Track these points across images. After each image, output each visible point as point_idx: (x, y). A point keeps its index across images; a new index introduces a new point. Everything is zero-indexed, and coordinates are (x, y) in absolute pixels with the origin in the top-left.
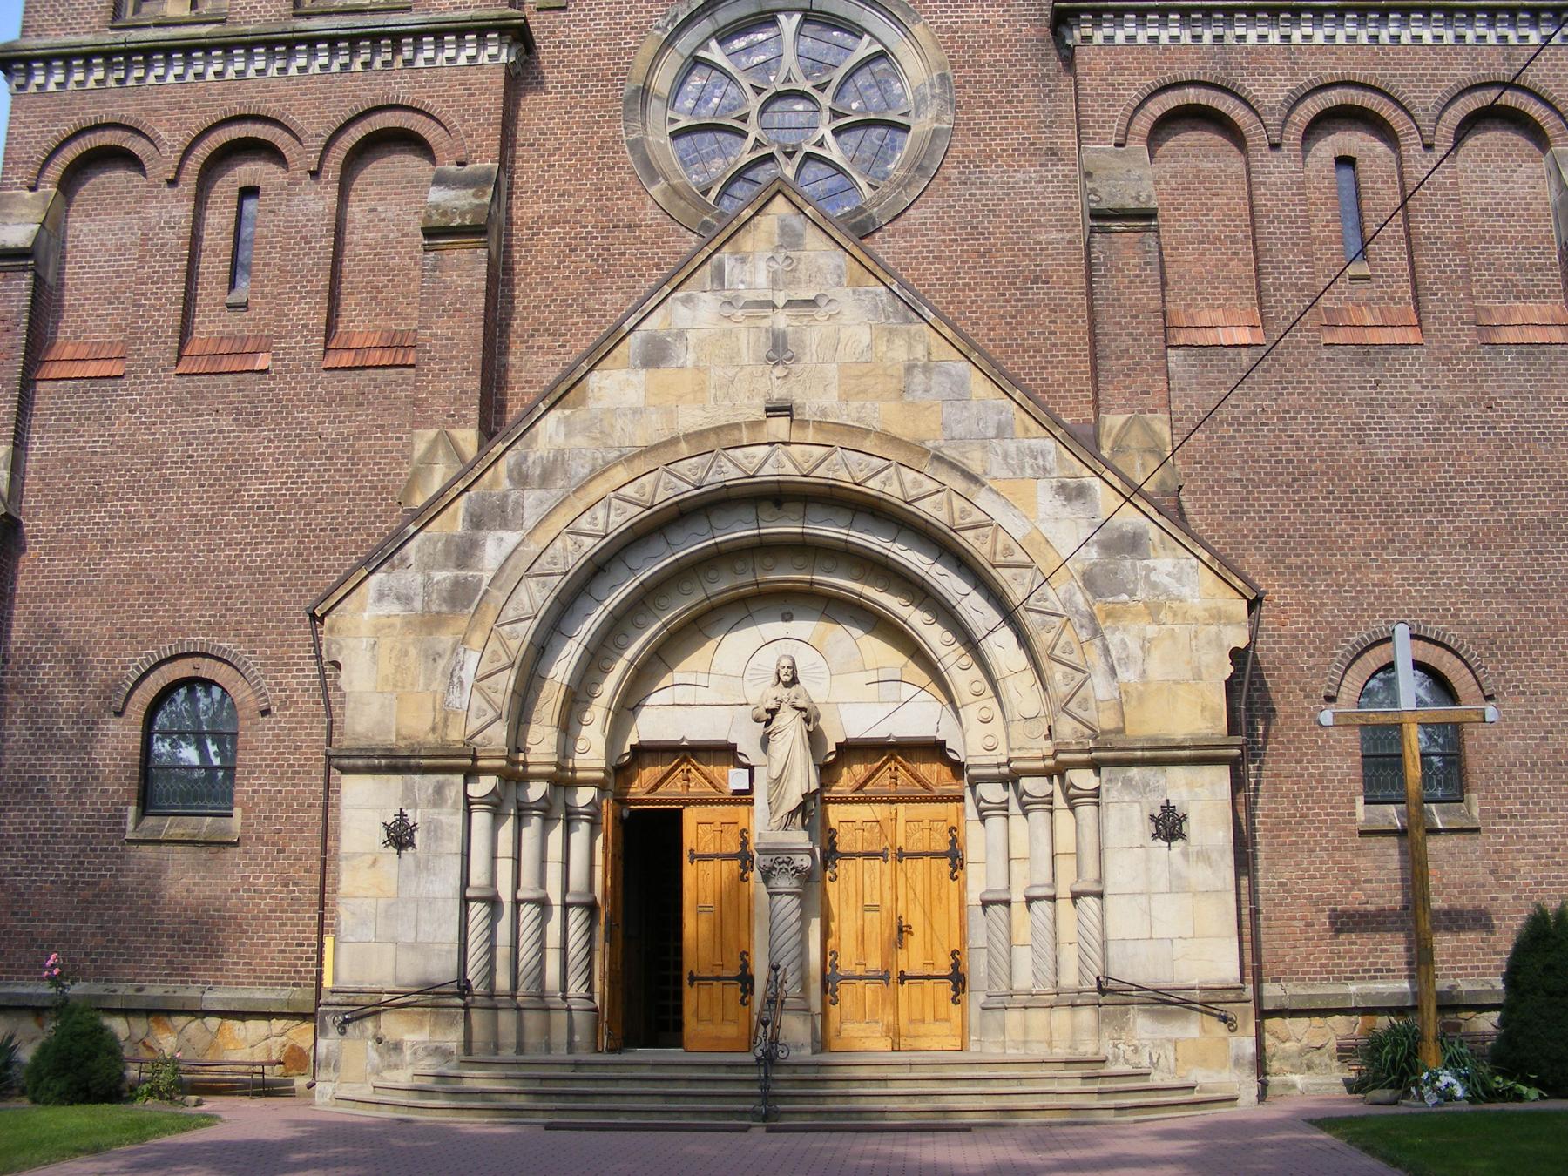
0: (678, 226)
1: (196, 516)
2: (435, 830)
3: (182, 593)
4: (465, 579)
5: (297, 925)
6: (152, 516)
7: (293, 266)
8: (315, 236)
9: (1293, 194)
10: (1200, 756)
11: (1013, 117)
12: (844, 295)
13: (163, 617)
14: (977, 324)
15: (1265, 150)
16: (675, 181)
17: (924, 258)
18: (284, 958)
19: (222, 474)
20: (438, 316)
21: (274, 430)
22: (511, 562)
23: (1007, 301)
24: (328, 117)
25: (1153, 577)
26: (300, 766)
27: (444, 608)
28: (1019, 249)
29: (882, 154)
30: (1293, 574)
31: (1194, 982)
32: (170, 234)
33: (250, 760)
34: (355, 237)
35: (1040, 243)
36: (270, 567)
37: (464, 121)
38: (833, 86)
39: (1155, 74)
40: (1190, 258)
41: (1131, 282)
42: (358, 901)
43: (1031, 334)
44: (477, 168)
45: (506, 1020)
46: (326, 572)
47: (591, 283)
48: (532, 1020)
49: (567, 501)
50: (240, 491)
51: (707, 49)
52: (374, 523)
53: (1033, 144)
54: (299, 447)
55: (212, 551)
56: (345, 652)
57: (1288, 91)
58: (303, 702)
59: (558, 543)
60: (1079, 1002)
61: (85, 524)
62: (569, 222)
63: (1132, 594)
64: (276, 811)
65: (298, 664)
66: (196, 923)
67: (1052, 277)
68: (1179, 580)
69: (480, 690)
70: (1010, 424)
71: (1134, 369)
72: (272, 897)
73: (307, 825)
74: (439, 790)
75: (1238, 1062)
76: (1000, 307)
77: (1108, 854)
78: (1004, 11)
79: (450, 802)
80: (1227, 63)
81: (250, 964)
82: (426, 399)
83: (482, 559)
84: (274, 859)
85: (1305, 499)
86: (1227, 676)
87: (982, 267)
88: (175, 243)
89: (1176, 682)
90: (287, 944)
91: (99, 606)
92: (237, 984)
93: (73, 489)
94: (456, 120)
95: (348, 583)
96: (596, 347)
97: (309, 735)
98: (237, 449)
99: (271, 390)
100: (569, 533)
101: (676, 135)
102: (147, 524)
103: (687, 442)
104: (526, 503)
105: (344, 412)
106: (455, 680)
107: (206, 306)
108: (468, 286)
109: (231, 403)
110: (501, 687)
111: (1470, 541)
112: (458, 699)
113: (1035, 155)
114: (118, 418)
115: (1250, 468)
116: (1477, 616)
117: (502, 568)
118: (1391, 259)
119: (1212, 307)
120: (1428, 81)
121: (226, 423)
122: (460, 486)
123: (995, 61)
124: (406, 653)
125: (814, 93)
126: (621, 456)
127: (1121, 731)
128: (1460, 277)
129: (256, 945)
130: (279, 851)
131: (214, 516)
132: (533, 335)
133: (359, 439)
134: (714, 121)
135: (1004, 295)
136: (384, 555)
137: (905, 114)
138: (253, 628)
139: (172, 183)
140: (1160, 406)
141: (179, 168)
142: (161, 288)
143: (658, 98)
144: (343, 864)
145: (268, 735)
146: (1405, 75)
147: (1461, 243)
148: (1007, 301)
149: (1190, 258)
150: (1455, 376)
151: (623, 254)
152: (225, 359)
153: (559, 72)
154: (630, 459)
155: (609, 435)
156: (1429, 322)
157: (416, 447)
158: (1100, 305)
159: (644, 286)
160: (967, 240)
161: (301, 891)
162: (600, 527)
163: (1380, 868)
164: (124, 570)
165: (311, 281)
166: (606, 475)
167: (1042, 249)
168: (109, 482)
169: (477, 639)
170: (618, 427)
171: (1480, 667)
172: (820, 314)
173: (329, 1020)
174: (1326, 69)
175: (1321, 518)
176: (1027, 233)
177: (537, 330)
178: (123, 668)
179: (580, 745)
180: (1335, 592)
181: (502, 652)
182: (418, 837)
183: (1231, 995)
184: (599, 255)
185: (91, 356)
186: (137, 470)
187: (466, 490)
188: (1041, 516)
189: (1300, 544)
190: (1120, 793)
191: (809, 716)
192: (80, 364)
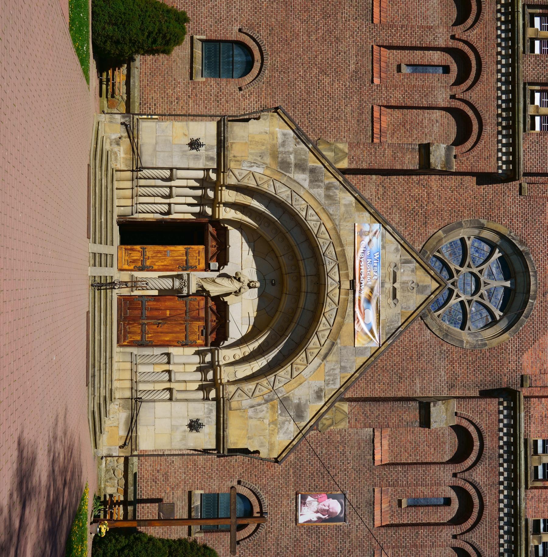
0: (425, 241)
1: (316, 57)
2: (197, 157)
3: (286, 54)
5: (162, 103)
6: (316, 39)
7: (416, 91)
8: (427, 99)
9: (435, 481)
10: (220, 437)
11: (468, 372)
12: (398, 310)
13: (277, 46)
15: (454, 471)
16: (444, 240)
17: (410, 336)
19: (333, 67)
20: (393, 151)
21: (349, 87)
22: (297, 185)
23: (392, 367)
24: (478, 100)
25: (287, 423)
26: (221, 103)
27: (280, 159)
28: (413, 372)
29: (453, 321)
30: (286, 471)
31: (139, 433)
32: (431, 38)
34: (426, 114)
35: (415, 380)
36: (296, 88)
37: (474, 157)
38: (482, 301)
39: (486, 429)
40: (409, 438)
41: (400, 416)
42: (171, 129)
43: (379, 375)
44: (453, 163)
45: (128, 184)
46: (293, 111)
47: (403, 209)
48: (128, 193)
49: (319, 205)
50: (326, 74)
51: (499, 252)
52: (312, 128)
53: (456, 379)
54: (342, 98)
55: (302, 65)
56: (264, 121)
57: (479, 483)
59: (304, 202)
60: (133, 391)
61: (314, 12)
62: (429, 199)
63: (281, 415)
64: (204, 94)
65: (259, 101)
66: (162, 64)
68: (285, 432)
69: (248, 174)
70: (346, 371)
71: (365, 415)
73: (199, 106)
74: (212, 159)
75: (110, 449)
76: (390, 364)
77: (186, 403)
78: (514, 370)
79: (208, 163)
80: (491, 458)
82: (360, 148)
83: (298, 173)
85: (314, 477)
86: (250, 449)
87: (406, 358)
88: (428, 41)
89: (247, 430)
90: (155, 100)
91: (282, 20)
92: (140, 81)
93: (328, 6)
94: (474, 154)
95: (290, 121)
96: (379, 215)
98: (342, 72)
99: (365, 85)
100: (307, 206)
101: (462, 240)
102: (313, 38)
103: (341, 250)
104: (319, 189)
105: (355, 115)
106: (253, 164)
107: (400, 55)
108: (405, 162)
109: (360, 69)
110: (250, 182)
111: (297, 540)
112: (245, 166)
113: (452, 379)
114: (356, 22)
115: (326, 457)
116: (269, 540)
117: (295, 181)
118: (408, 517)
119: (389, 445)
120: (484, 540)
121: (353, 67)
122: (326, 164)
123: (492, 366)
124: (263, 145)
125: (479, 294)
127: (230, 409)
128: (401, 544)
129: (155, 88)
131: (316, 64)
132: (383, 186)
133: (345, 121)
134: (468, 254)
135: (395, 365)
136: (300, 136)
137: (469, 329)
138: (273, 83)
139: (453, 37)
140: (351, 425)
141: (460, 40)
142: (409, 36)
143: (479, 233)
144: (185, 123)
146: (486, 530)
147: (415, 546)
148: (392, 367)
149: (409, 438)
150: (361, 539)
151: (415, 221)
152: (378, 65)
153: (492, 193)
154: (335, 229)
155: (345, 221)
156: (383, 530)
157: (341, 144)
159: (401, 229)
161: (175, 104)
162: (309, 218)
163: (177, 499)
164: (296, 29)
165: (409, 98)
168: (331, 20)
169: (268, 172)
170: (348, 224)
171: (250, 540)
172: (390, 300)
173: (127, 119)
174: (489, 498)
175: (307, 482)
176: (419, 375)
177: (385, 188)
179: (228, 209)
180: (279, 486)
181: (263, 181)
182: (194, 151)
183: (134, 447)
184: (415, 211)
185: (382, 9)
186: (335, 32)
187: (325, 167)
188: (310, 382)
189: (297, 474)
190: (207, 408)
191: (237, 293)
192: (378, 4)
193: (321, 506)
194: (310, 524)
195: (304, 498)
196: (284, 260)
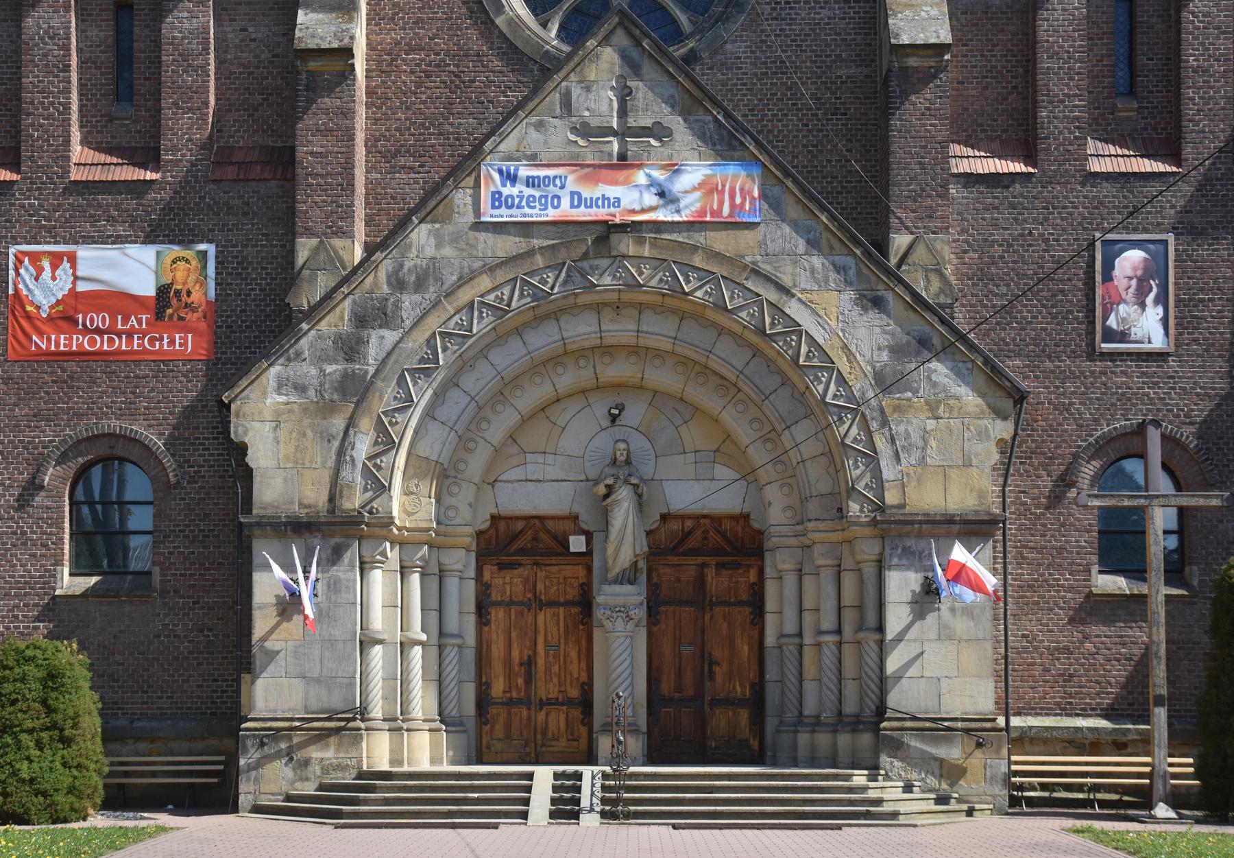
4: (353, 371)
14: (784, 152)
18: (202, 692)
23: (809, 131)
26: (209, 531)
27: (336, 397)
33: (165, 526)
35: (841, 77)
40: (974, 92)
56: (250, 434)
58: (209, 477)
63: (915, 392)
64: (190, 569)
66: (123, 664)
67: (850, 109)
72: (189, 642)
73: (218, 580)
81: (172, 697)
84: (190, 609)
87: (789, 99)
90: (204, 680)
97: (215, 504)
103: (542, 254)
118: (1157, 92)
124: (305, 435)
126: (484, 266)
127: (903, 506)
130: (194, 603)
133: (246, 246)
145: (180, 504)
150: (1208, 201)
158: (894, 136)
160: (776, 73)
166: (472, 282)
167: (842, 82)
176: (829, 68)
178: (44, 447)
193: (1130, 296)
194: (1172, 322)
195: (1109, 335)
196: (566, 379)
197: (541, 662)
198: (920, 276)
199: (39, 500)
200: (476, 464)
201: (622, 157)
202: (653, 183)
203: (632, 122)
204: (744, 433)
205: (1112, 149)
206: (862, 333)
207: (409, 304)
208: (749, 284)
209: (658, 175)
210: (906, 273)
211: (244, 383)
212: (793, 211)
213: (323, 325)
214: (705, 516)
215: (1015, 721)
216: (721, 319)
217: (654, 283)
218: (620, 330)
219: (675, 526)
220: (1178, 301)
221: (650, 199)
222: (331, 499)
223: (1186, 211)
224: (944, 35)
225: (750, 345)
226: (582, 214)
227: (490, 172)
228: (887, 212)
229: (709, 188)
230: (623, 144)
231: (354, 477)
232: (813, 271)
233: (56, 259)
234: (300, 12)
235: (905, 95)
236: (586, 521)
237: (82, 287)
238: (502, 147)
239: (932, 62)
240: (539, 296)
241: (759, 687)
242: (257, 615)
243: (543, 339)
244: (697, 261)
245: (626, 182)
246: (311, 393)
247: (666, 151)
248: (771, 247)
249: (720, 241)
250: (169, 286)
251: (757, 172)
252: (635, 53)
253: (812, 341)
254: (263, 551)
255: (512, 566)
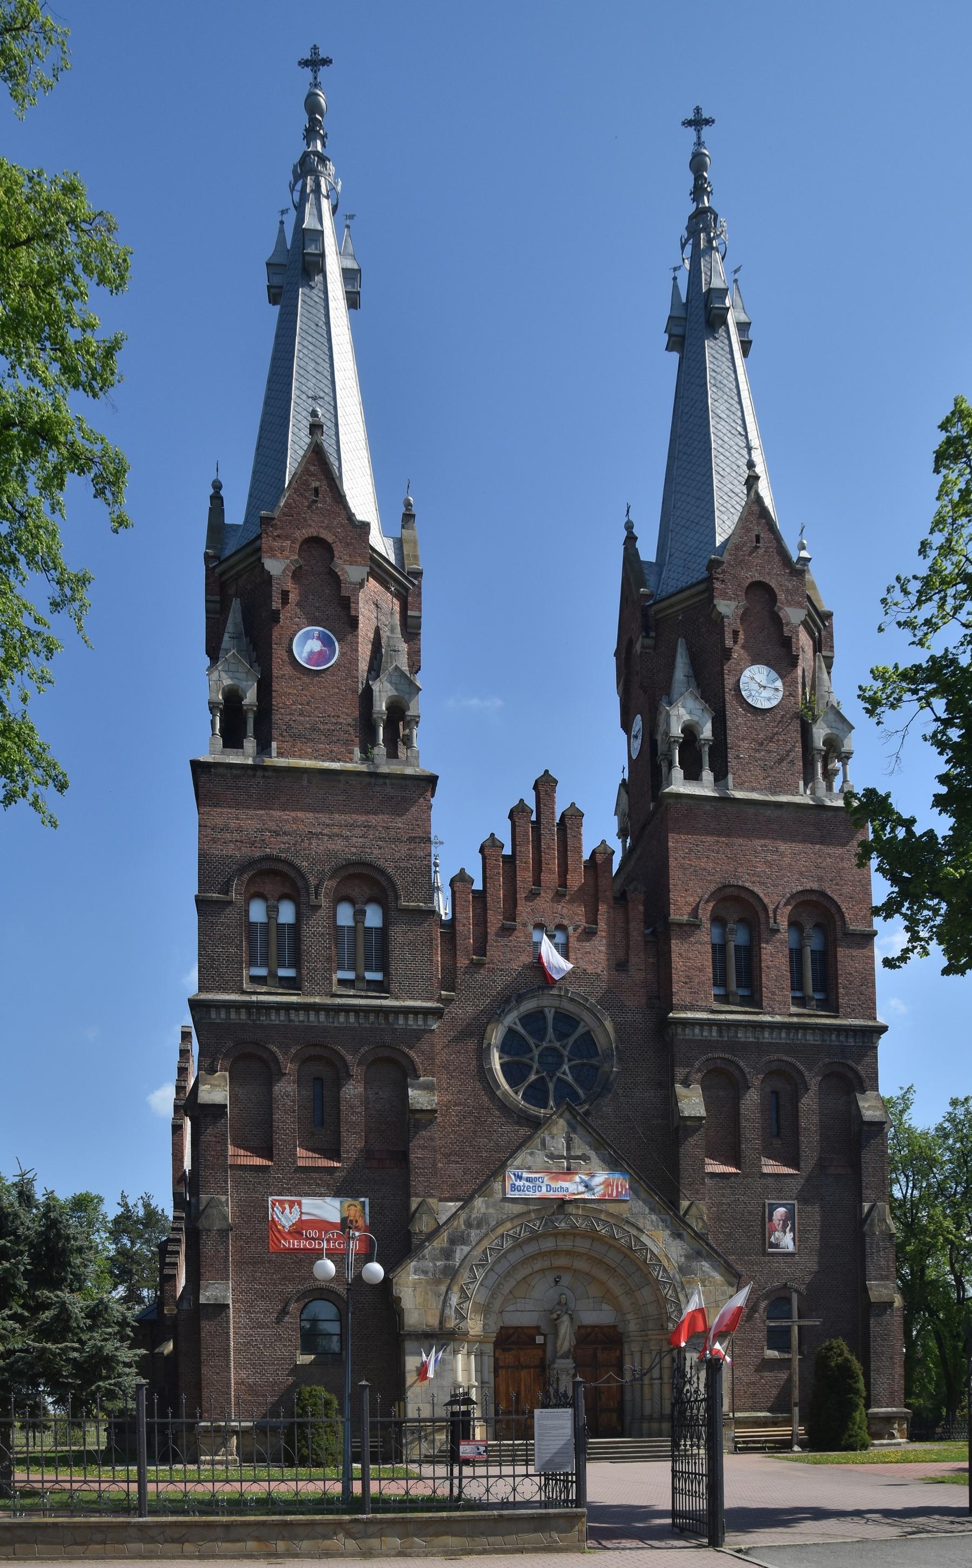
63: (696, 1275)
154: (512, 1219)
193: (780, 1228)
194: (797, 1239)
195: (772, 1245)
196: (538, 1266)
197: (523, 1394)
198: (694, 1220)
199: (287, 1319)
200: (497, 1305)
201: (568, 1169)
202: (582, 1181)
203: (572, 1154)
204: (617, 1290)
205: (771, 1162)
206: (673, 1249)
207: (474, 1234)
208: (625, 1227)
209: (584, 1177)
210: (688, 1219)
211: (399, 1269)
212: (643, 1195)
213: (435, 1244)
214: (596, 1326)
215: (738, 1415)
216: (612, 1242)
217: (583, 1226)
218: (566, 1244)
219: (583, 1331)
220: (799, 1230)
221: (581, 1188)
222: (441, 1323)
223: (801, 1190)
224: (702, 1112)
225: (623, 1253)
226: (552, 1195)
227: (510, 1174)
228: (678, 1191)
229: (607, 1184)
230: (569, 1163)
231: (450, 1312)
232: (652, 1221)
233: (292, 1204)
234: (409, 1090)
235: (686, 1139)
236: (545, 1328)
237: (304, 1217)
238: (515, 1163)
239: (697, 1124)
240: (532, 1231)
241: (621, 1403)
242: (408, 1375)
243: (530, 1249)
244: (603, 1217)
245: (570, 1181)
246: (430, 1274)
247: (588, 1167)
248: (634, 1210)
249: (612, 1208)
250: (347, 1218)
251: (627, 1177)
252: (573, 1122)
253: (652, 1252)
254: (409, 1345)
255: (509, 1350)
